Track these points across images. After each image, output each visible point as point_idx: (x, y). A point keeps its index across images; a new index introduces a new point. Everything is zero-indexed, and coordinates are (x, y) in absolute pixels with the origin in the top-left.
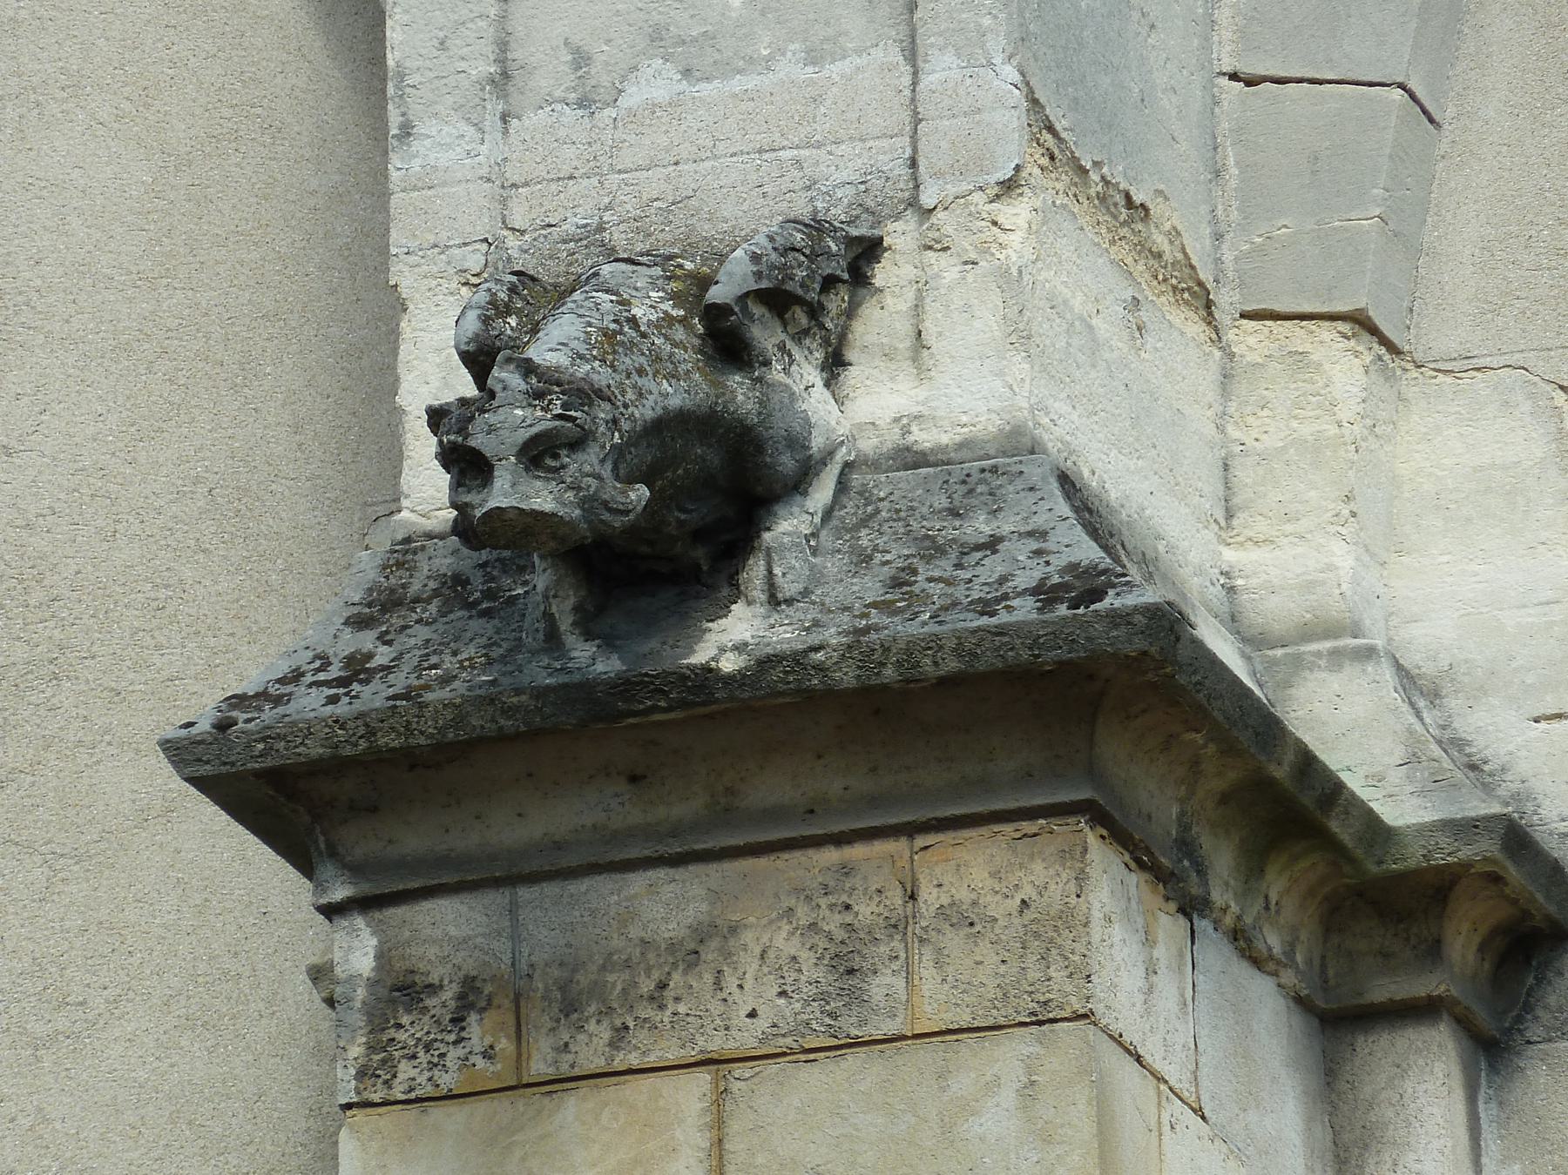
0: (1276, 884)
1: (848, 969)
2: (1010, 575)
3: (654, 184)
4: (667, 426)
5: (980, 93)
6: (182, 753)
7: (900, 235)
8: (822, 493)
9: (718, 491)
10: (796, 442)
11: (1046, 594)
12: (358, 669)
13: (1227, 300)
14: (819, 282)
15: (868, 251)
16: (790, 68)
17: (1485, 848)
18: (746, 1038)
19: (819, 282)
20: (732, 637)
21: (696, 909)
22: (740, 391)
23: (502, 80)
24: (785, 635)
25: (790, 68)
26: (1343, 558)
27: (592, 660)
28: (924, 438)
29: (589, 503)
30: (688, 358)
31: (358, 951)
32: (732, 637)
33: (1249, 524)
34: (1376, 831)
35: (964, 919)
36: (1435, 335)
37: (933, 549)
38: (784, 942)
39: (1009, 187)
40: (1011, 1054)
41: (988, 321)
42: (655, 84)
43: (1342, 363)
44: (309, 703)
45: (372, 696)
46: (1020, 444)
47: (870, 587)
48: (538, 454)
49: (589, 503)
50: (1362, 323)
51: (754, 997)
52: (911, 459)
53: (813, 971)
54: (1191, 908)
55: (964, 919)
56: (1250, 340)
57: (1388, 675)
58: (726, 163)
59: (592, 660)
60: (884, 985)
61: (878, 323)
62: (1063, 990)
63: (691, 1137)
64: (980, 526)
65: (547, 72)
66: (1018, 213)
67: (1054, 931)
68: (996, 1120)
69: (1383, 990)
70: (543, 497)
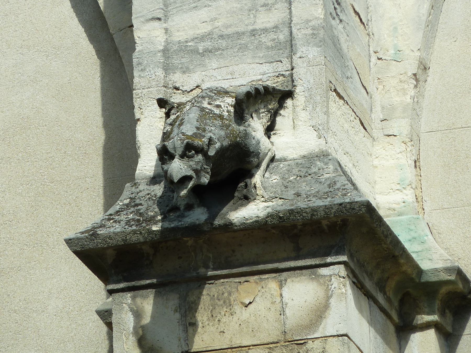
2: (312, 197)
9: (233, 168)
14: (269, 99)
20: (252, 211)
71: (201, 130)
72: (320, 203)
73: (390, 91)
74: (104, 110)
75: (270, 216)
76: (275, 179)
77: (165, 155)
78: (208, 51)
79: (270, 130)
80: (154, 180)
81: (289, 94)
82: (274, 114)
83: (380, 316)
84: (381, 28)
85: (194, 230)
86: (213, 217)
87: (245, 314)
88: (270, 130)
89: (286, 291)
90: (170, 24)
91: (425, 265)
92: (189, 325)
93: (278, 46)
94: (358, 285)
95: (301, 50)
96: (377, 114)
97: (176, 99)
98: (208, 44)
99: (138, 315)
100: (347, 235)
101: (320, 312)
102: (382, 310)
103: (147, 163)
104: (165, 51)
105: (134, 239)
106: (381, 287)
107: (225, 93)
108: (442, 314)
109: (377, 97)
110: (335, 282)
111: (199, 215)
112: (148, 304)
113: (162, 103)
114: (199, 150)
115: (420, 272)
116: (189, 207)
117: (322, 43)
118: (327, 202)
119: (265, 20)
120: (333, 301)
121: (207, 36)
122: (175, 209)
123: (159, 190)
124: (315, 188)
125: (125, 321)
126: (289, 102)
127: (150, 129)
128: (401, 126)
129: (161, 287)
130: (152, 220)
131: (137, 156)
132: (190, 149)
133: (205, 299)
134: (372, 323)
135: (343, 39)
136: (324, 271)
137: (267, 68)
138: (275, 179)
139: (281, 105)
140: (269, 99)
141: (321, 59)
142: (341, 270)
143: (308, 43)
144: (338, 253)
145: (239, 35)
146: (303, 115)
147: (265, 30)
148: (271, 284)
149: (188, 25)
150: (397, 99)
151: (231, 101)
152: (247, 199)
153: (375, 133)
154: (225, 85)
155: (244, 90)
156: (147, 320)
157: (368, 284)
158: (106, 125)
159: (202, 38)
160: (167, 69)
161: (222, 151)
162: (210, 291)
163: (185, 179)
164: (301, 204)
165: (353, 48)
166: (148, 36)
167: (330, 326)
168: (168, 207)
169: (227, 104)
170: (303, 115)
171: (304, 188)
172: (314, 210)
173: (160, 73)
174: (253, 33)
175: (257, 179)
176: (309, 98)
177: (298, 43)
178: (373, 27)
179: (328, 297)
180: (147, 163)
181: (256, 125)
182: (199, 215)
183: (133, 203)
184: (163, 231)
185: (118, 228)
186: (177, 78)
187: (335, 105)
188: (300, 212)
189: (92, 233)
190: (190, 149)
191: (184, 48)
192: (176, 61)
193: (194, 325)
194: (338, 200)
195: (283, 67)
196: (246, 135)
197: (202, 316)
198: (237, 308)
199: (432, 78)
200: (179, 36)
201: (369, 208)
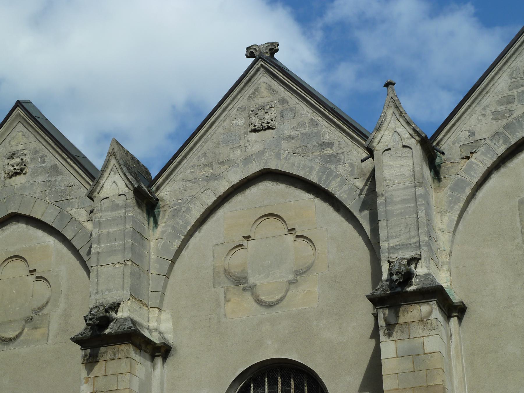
0: (148, 347)
1: (115, 354)
2: (427, 284)
3: (106, 299)
4: (102, 317)
5: (128, 293)
6: (71, 339)
7: (122, 303)
8: (115, 321)
9: (408, 277)
10: (112, 318)
11: (127, 328)
12: (84, 333)
13: (149, 307)
14: (115, 307)
15: (120, 304)
16: (115, 292)
17: (163, 344)
18: (108, 359)
19: (115, 307)
20: (413, 288)
21: (105, 350)
22: (108, 314)
23: (97, 293)
24: (111, 331)
25: (115, 292)
26: (156, 324)
27: (98, 333)
28: (122, 317)
29: (94, 323)
30: (104, 312)
31: (83, 353)
32: (107, 331)
33: (150, 322)
34: (155, 343)
35: (122, 350)
36: (164, 309)
37: (121, 325)
38: (111, 352)
39: (129, 300)
40: (125, 360)
41: (127, 309)
42: (107, 293)
43: (157, 311)
44: (80, 336)
45: (84, 335)
46: (129, 317)
47: (117, 328)
48: (90, 319)
49: (94, 323)
50: (158, 308)
51: (108, 356)
52: (121, 319)
53: (112, 354)
54: (140, 349)
55: (122, 350)
56: (151, 309)
57: (158, 332)
58: (110, 298)
59: (98, 333)
60: (117, 355)
61: (120, 309)
62: (128, 355)
63: (104, 366)
64: (125, 323)
65: (100, 292)
66: (129, 302)
67: (128, 351)
68: (123, 364)
69: (157, 354)
70: (91, 322)
71: (400, 268)
72: (429, 286)
73: (443, 258)
74: (371, 264)
75: (417, 289)
76: (417, 280)
77: (391, 274)
78: (399, 249)
79: (416, 268)
80: (387, 281)
81: (420, 259)
82: (416, 264)
83: (444, 314)
84: (440, 243)
85: (398, 293)
86: (403, 289)
87: (411, 314)
88: (416, 268)
89: (421, 308)
90: (389, 242)
91: (454, 301)
92: (397, 317)
93: (416, 247)
94: (439, 306)
95: (423, 248)
96: (440, 264)
97: (392, 260)
98: (399, 247)
99: (384, 314)
100: (435, 293)
101: (430, 313)
102: (444, 313)
103: (385, 276)
104: (388, 249)
105: (383, 295)
106: (444, 306)
107: (404, 259)
108: (458, 313)
109: (440, 259)
110: (434, 306)
111: (399, 289)
112: (387, 312)
113: (389, 261)
114: (400, 273)
115: (453, 303)
116: (396, 287)
117: (427, 246)
118: (431, 285)
119: (413, 241)
120: (433, 310)
121: (399, 245)
122: (393, 288)
123: (388, 283)
124: (428, 282)
125: (381, 316)
126: (420, 261)
127: (385, 268)
128: (446, 267)
129: (390, 307)
130: (387, 291)
131: (382, 275)
132: (398, 273)
133: (401, 310)
134: (442, 315)
135: (432, 245)
136: (431, 303)
137: (414, 252)
138: (417, 280)
139: (418, 262)
140: (415, 260)
141: (428, 250)
142: (435, 302)
143: (424, 246)
144: (434, 298)
145: (407, 244)
146: (424, 264)
147: (413, 243)
148: (418, 306)
149: (394, 242)
150: (445, 260)
151: (406, 261)
152: (411, 285)
153: (440, 268)
154: (404, 257)
155: (410, 258)
156: (387, 315)
157: (441, 306)
158: (372, 267)
159: (397, 245)
160: (389, 253)
161: (405, 273)
162: (402, 308)
163: (397, 280)
164: (425, 286)
165: (434, 247)
166: (384, 245)
167: (433, 316)
168: (391, 287)
169: (405, 262)
170: (424, 264)
171: (425, 282)
172: (428, 288)
173: (387, 254)
174: (410, 244)
175: (413, 280)
176: (425, 260)
177: (422, 246)
178: (438, 242)
179: (432, 309)
180: (385, 276)
181: (413, 267)
182: (399, 289)
183: (382, 287)
184: (390, 293)
185: (379, 293)
186: (391, 255)
187: (431, 262)
188: (425, 288)
189: (372, 294)
190: (398, 273)
191: (393, 248)
192: (391, 251)
193: (398, 316)
194: (434, 285)
195: (418, 252)
196: (411, 269)
197: (400, 314)
198: (409, 312)
199: (453, 255)
200: (391, 245)
201: (442, 286)
